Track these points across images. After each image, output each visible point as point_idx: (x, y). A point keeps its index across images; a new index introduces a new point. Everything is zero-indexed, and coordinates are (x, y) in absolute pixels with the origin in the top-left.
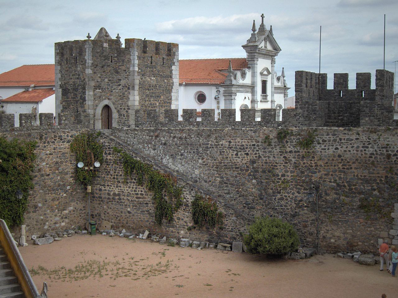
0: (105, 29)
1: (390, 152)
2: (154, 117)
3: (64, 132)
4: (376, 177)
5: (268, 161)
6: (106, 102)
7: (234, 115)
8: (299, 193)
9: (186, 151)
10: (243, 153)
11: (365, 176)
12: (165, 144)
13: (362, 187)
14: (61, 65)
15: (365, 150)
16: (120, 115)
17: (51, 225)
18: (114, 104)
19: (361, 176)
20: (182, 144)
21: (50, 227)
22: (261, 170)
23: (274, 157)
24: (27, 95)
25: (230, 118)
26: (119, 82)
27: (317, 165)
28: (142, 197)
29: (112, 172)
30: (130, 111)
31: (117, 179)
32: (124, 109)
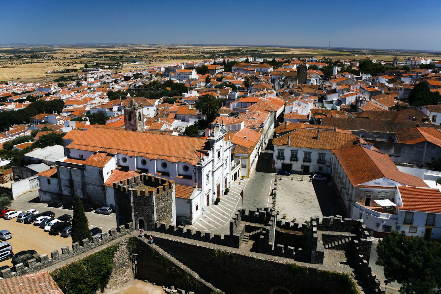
6: (141, 218)
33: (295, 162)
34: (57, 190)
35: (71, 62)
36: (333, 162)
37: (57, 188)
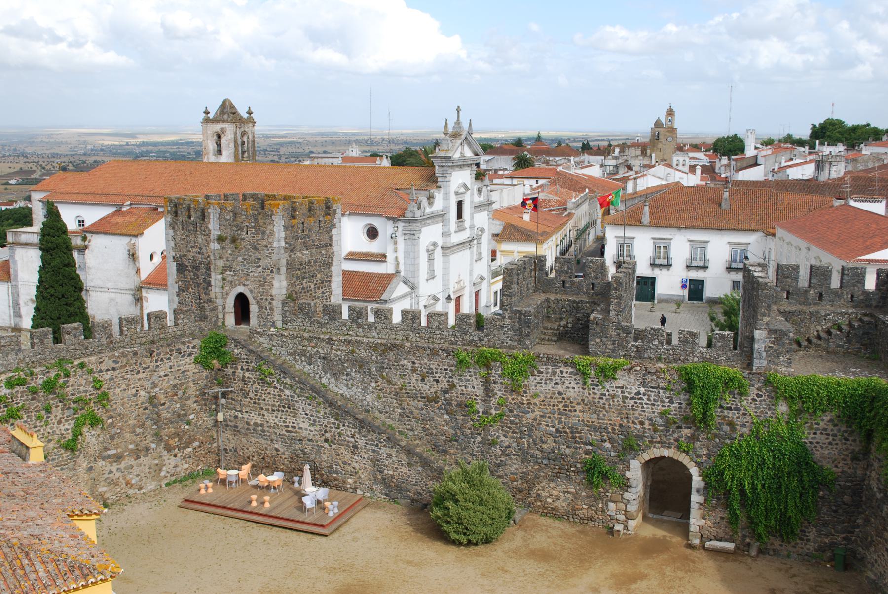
0: (230, 101)
1: (626, 394)
2: (308, 313)
3: (184, 343)
4: (607, 424)
5: (465, 392)
6: (240, 289)
7: (419, 318)
8: (505, 436)
9: (354, 370)
10: (432, 379)
11: (592, 422)
12: (324, 358)
13: (589, 435)
14: (174, 228)
15: (594, 389)
16: (261, 307)
17: (169, 470)
18: (251, 291)
19: (588, 422)
20: (347, 360)
21: (168, 472)
22: (456, 403)
23: (474, 388)
24: (119, 219)
25: (413, 323)
26: (258, 262)
27: (531, 403)
28: (293, 430)
29: (251, 395)
30: (274, 302)
31: (259, 404)
32: (266, 299)
33: (664, 271)
34: (7, 318)
35: (71, 162)
36: (772, 257)
37: (7, 311)
